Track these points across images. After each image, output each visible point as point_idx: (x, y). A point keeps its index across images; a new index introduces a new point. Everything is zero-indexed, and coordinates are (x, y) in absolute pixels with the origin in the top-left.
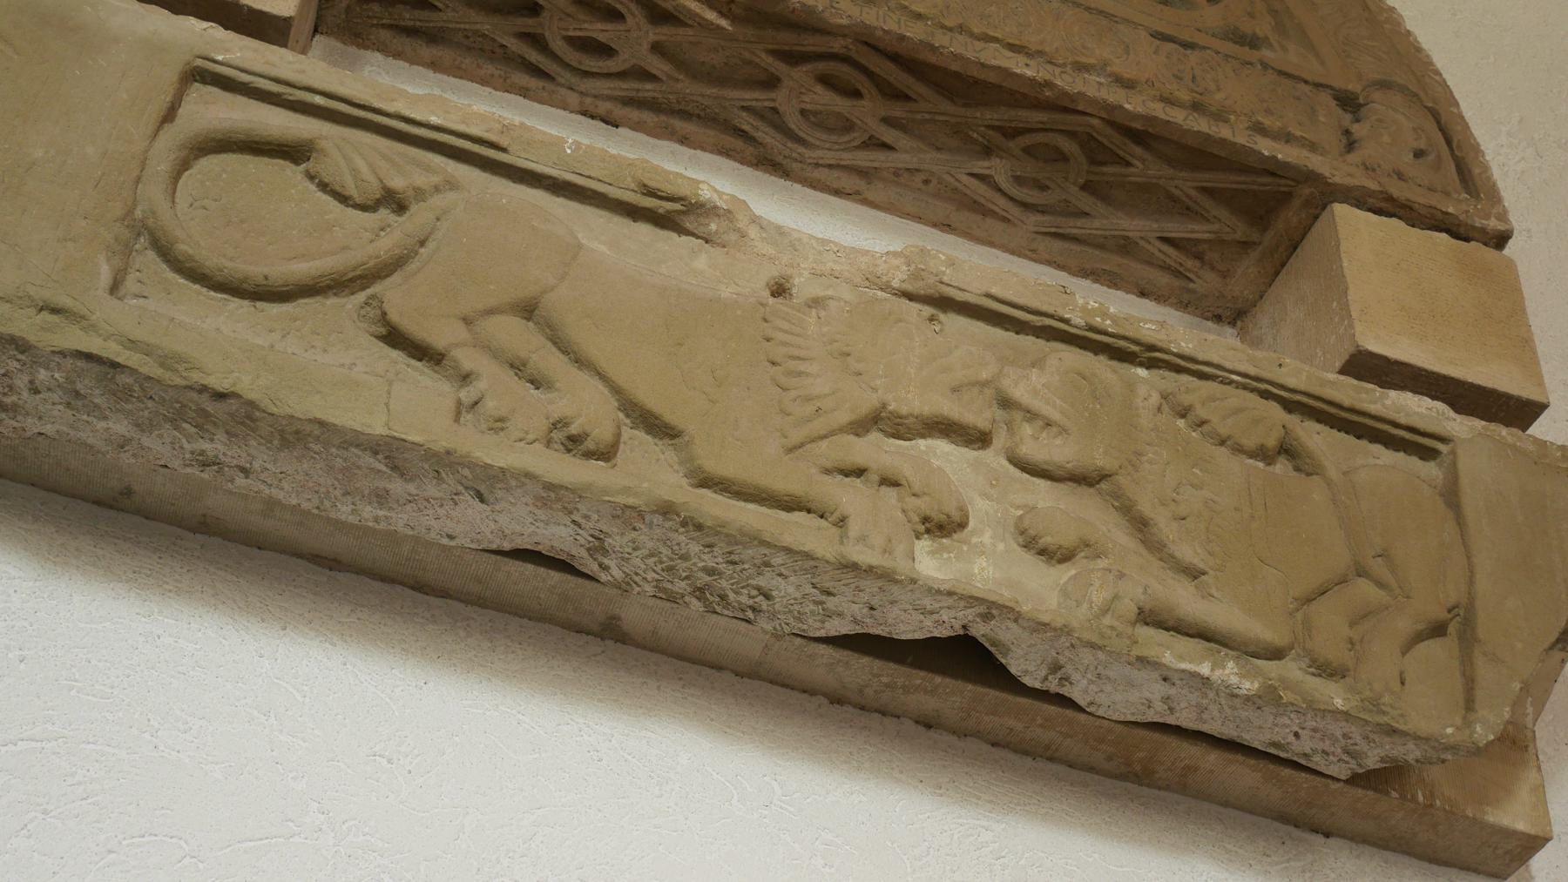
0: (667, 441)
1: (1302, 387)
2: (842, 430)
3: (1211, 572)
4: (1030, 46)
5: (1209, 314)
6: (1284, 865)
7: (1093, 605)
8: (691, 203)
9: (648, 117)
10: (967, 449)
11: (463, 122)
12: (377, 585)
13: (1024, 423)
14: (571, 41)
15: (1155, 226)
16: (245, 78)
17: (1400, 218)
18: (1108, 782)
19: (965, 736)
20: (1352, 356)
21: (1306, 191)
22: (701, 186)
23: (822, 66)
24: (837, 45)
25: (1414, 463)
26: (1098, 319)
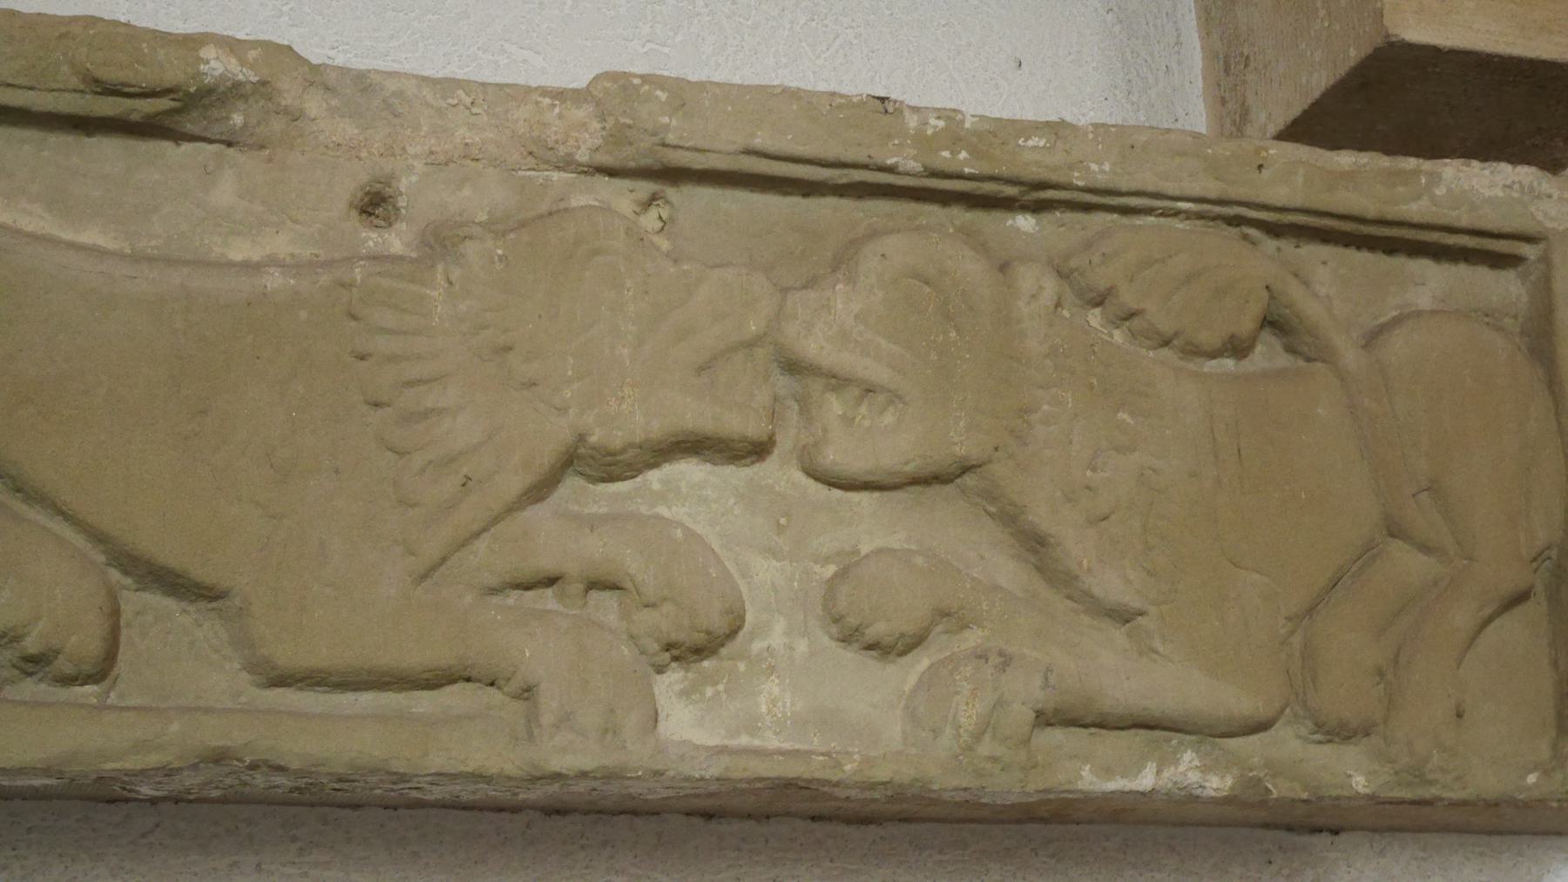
0: (202, 605)
1: (1298, 202)
2: (512, 509)
3: (1153, 610)
7: (962, 731)
8: (188, 94)
10: (732, 467)
13: (828, 395)
19: (768, 817)
25: (1481, 276)
26: (946, 154)
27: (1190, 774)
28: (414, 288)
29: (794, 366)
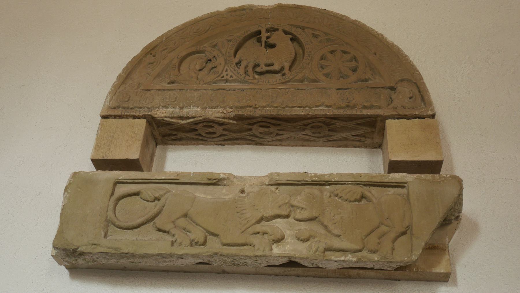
1: (367, 181)
2: (254, 224)
3: (342, 235)
4: (304, 106)
5: (373, 147)
6: (388, 290)
9: (229, 142)
11: (170, 176)
12: (177, 273)
13: (297, 210)
14: (207, 133)
15: (349, 134)
16: (126, 181)
17: (405, 118)
18: (342, 279)
19: (307, 277)
20: (389, 162)
21: (379, 119)
22: (220, 175)
23: (258, 124)
24: (259, 120)
26: (314, 178)
27: (350, 258)
28: (244, 199)
29: (293, 206)
